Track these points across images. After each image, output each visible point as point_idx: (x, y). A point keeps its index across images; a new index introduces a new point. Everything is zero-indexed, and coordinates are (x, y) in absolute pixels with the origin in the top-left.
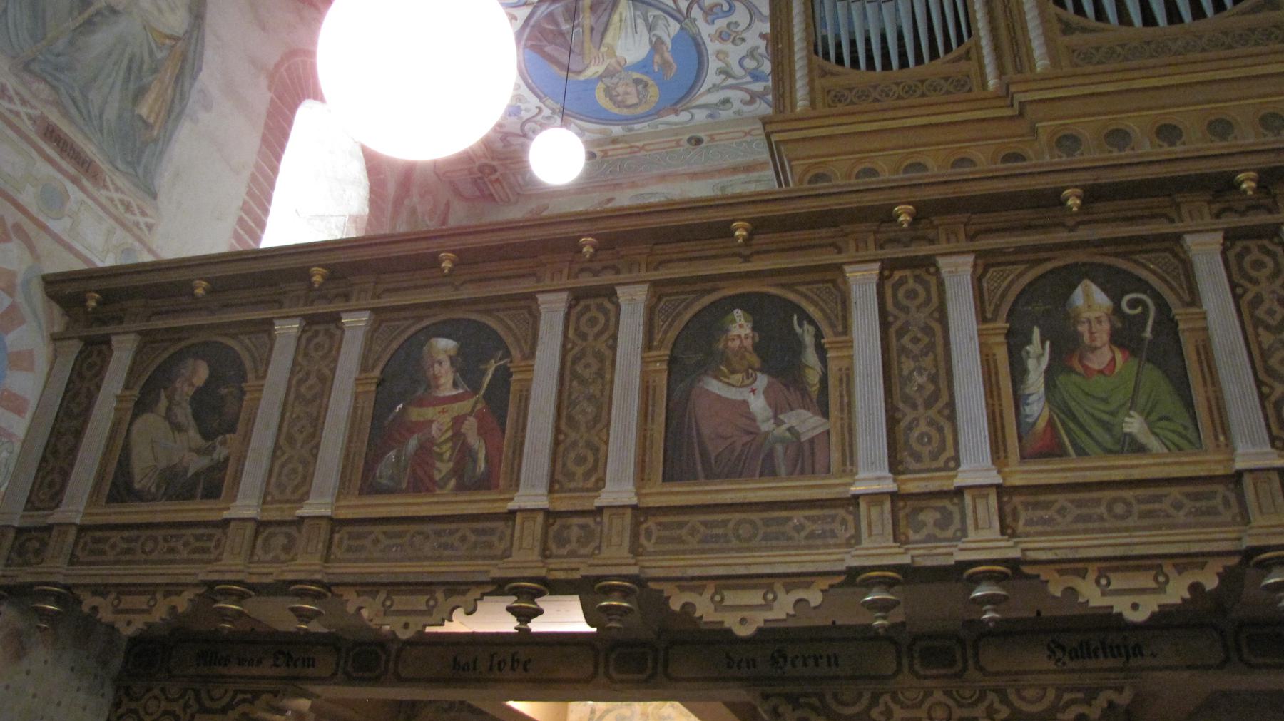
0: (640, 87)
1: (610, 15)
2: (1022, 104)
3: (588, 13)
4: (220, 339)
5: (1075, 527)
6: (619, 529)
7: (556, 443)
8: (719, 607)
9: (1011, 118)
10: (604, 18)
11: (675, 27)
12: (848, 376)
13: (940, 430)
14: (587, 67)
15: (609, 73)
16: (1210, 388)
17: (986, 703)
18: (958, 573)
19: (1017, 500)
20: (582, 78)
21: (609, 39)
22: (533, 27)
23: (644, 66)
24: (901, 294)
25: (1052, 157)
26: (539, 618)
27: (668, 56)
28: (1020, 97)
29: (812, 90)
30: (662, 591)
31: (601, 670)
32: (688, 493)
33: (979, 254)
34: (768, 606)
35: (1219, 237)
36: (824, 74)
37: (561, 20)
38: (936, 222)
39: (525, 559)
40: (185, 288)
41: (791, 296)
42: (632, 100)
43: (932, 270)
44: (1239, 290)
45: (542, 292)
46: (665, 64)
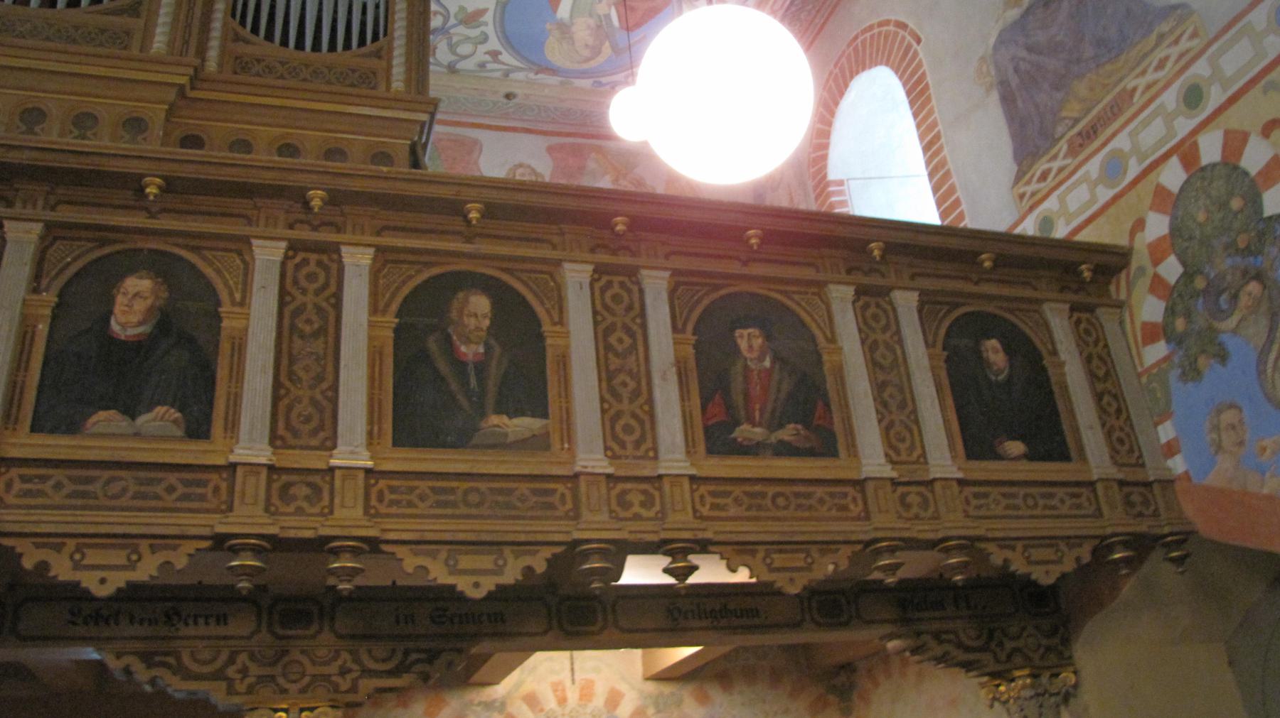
4: (176, 251)
5: (179, 505)
6: (255, 487)
7: (276, 399)
8: (77, 566)
12: (240, 345)
13: (911, 431)
16: (20, 379)
17: (339, 662)
18: (320, 546)
19: (382, 483)
24: (322, 279)
25: (62, 135)
26: (696, 573)
30: (13, 548)
31: (264, 625)
32: (405, 459)
33: (380, 250)
34: (131, 566)
35: (590, 268)
36: (237, 38)
38: (16, 186)
39: (681, 522)
40: (456, 209)
41: (789, 303)
43: (335, 256)
44: (333, 301)
45: (571, 261)
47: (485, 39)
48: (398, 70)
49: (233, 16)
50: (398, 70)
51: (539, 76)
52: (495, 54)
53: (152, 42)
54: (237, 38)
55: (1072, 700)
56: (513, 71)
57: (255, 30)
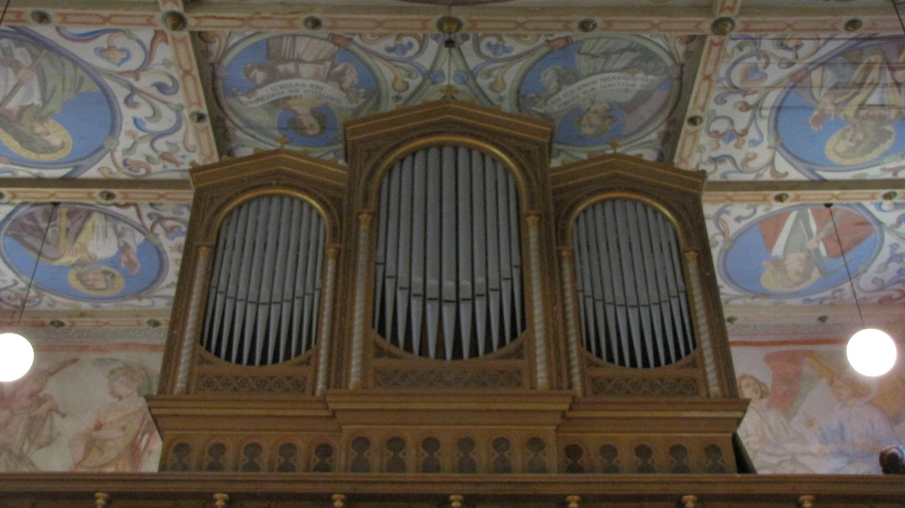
0: (108, 277)
1: (84, 223)
2: (334, 412)
3: (64, 218)
9: (326, 417)
10: (79, 223)
11: (140, 238)
14: (62, 256)
15: (81, 263)
20: (56, 263)
21: (82, 238)
22: (14, 221)
23: (113, 262)
27: (134, 258)
28: (332, 406)
29: (190, 374)
36: (203, 361)
37: (40, 220)
42: (101, 284)
46: (130, 263)
48: (712, 376)
49: (589, 348)
50: (712, 376)
51: (756, 300)
53: (536, 379)
54: (591, 364)
55: (896, 89)
56: (731, 299)
57: (599, 354)
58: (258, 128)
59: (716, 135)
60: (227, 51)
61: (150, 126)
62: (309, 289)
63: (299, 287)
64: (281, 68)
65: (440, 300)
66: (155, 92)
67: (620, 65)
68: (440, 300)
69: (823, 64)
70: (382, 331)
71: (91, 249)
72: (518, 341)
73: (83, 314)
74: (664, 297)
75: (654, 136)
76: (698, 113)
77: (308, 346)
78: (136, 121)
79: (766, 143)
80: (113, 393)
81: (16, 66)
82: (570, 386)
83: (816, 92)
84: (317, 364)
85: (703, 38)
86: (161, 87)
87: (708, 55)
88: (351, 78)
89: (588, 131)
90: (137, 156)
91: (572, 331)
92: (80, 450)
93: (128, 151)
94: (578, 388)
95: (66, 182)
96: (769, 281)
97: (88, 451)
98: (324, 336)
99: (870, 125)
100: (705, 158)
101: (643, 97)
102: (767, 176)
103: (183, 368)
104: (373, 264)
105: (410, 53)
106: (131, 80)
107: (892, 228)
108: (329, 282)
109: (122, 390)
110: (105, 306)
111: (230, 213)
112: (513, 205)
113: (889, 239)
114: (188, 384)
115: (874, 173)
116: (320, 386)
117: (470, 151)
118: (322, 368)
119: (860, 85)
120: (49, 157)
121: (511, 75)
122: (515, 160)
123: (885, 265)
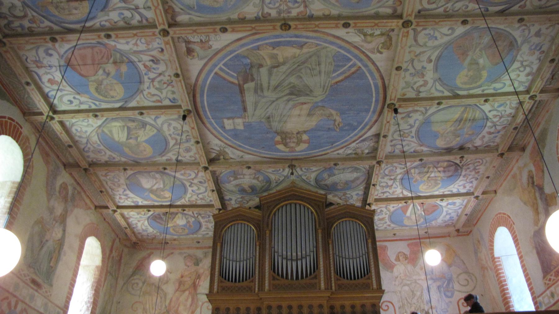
2: (261, 299)
11: (193, 219)
15: (174, 226)
21: (175, 220)
23: (184, 226)
28: (261, 297)
36: (221, 282)
46: (190, 226)
47: (386, 222)
48: (374, 282)
50: (374, 282)
52: (389, 225)
58: (232, 191)
59: (383, 187)
60: (221, 173)
61: (197, 192)
62: (251, 256)
63: (248, 255)
64: (239, 177)
65: (292, 260)
66: (199, 183)
67: (348, 171)
68: (292, 260)
69: (414, 168)
70: (274, 271)
71: (178, 222)
72: (316, 273)
73: (175, 240)
74: (361, 255)
75: (362, 188)
76: (375, 183)
77: (252, 276)
78: (192, 191)
79: (399, 187)
80: (186, 265)
81: (156, 178)
82: (331, 289)
83: (413, 175)
84: (255, 282)
85: (374, 166)
86: (200, 182)
87: (376, 170)
88: (261, 178)
89: (339, 187)
90: (192, 199)
91: (332, 269)
92: (177, 285)
93: (190, 198)
94: (333, 288)
95: (170, 206)
96: (406, 222)
97: (180, 285)
98: (257, 272)
99: (432, 182)
100: (380, 192)
101: (357, 179)
102: (401, 196)
103: (216, 284)
104: (271, 248)
105: (280, 172)
106: (191, 181)
107: (445, 207)
108: (258, 254)
109: (189, 264)
110: (181, 237)
111: (226, 230)
112: (314, 224)
113: (445, 209)
114: (218, 289)
115: (436, 193)
116: (257, 289)
117: (300, 205)
118: (257, 283)
119: (428, 172)
120: (165, 200)
121: (313, 176)
122: (314, 209)
123: (445, 216)
